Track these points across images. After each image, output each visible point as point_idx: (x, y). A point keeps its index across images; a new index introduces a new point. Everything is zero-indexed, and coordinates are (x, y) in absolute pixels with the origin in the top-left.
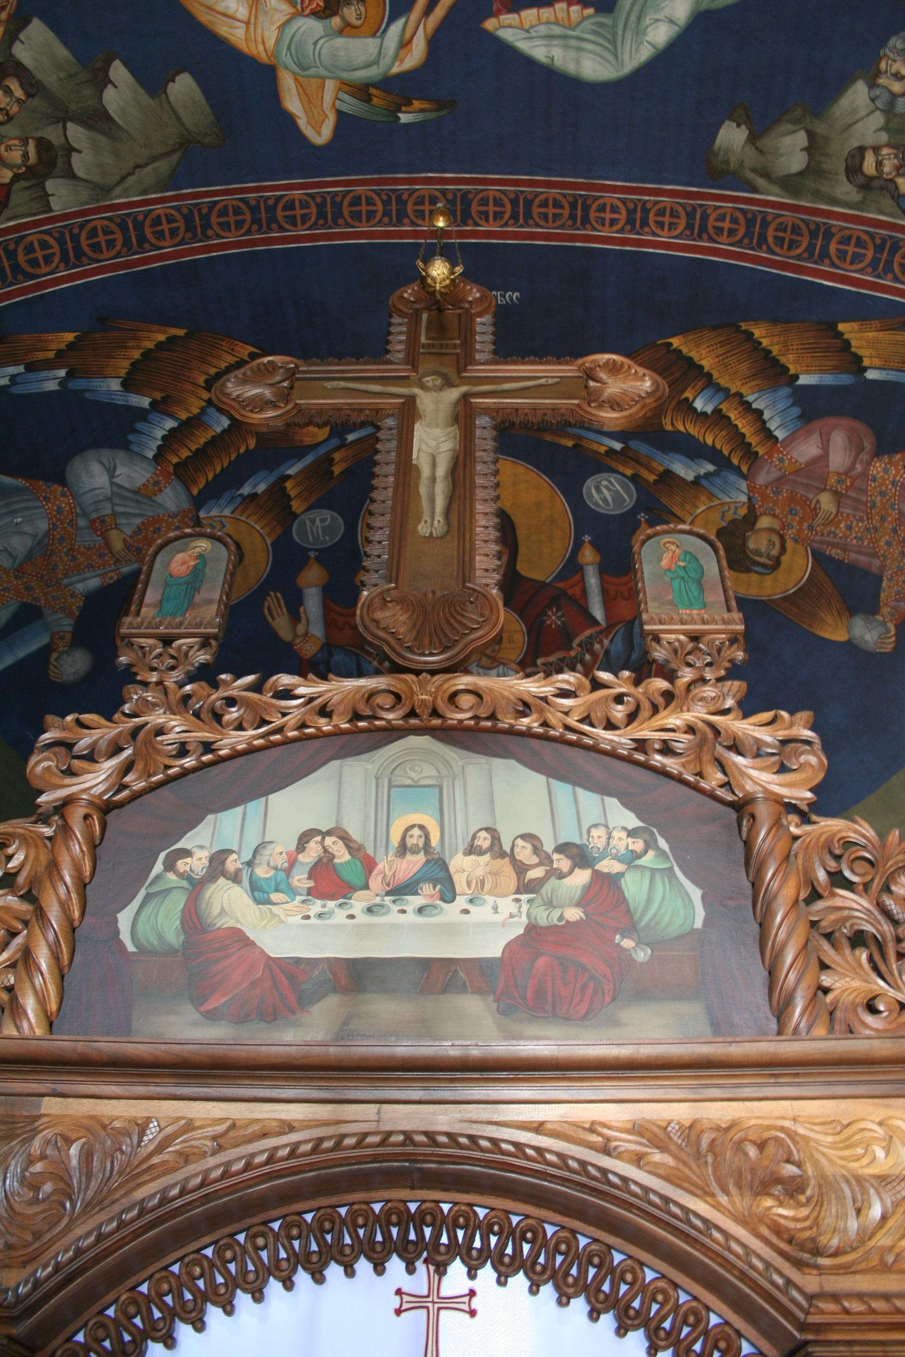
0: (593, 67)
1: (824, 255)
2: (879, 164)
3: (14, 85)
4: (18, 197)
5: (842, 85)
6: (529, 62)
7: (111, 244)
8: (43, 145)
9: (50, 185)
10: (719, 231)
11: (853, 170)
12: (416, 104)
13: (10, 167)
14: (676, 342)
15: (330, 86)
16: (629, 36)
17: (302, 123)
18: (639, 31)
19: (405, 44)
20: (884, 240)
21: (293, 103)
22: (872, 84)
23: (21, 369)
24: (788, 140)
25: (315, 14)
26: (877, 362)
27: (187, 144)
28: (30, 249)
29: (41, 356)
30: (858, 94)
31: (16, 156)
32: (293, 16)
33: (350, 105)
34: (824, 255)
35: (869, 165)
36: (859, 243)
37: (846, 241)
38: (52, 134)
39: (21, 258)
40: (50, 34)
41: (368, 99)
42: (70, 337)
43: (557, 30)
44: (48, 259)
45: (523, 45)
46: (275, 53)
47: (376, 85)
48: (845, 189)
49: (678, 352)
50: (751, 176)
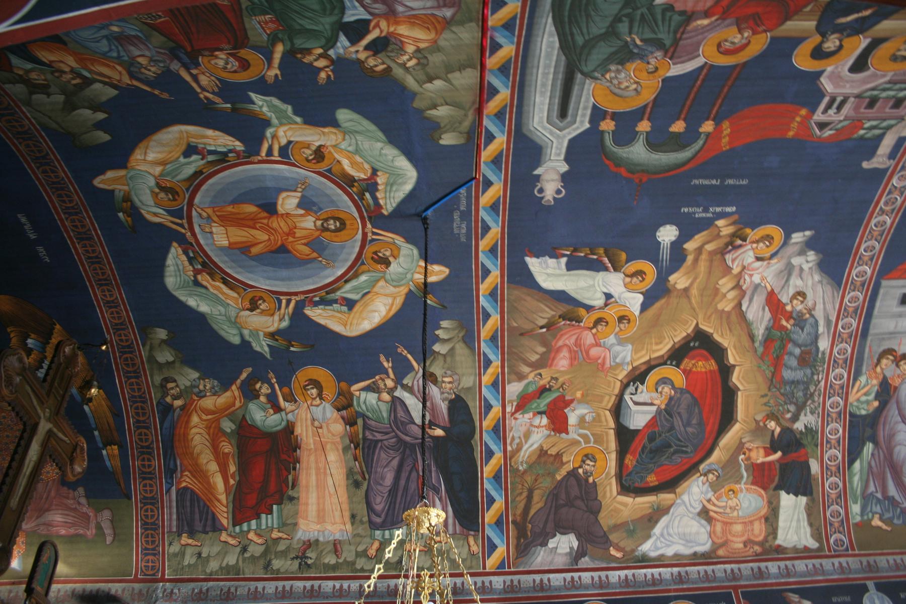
0: (170, 282)
1: (128, 378)
2: (172, 388)
5: (195, 368)
6: (164, 258)
10: (120, 335)
11: (167, 380)
14: (58, 327)
15: (126, 188)
17: (102, 177)
18: (190, 295)
20: (145, 397)
21: (110, 174)
22: (199, 378)
24: (168, 354)
26: (93, 408)
30: (195, 375)
32: (154, 176)
34: (128, 378)
35: (170, 385)
36: (139, 389)
37: (138, 384)
45: (170, 256)
46: (133, 168)
48: (158, 379)
49: (54, 329)
50: (148, 343)
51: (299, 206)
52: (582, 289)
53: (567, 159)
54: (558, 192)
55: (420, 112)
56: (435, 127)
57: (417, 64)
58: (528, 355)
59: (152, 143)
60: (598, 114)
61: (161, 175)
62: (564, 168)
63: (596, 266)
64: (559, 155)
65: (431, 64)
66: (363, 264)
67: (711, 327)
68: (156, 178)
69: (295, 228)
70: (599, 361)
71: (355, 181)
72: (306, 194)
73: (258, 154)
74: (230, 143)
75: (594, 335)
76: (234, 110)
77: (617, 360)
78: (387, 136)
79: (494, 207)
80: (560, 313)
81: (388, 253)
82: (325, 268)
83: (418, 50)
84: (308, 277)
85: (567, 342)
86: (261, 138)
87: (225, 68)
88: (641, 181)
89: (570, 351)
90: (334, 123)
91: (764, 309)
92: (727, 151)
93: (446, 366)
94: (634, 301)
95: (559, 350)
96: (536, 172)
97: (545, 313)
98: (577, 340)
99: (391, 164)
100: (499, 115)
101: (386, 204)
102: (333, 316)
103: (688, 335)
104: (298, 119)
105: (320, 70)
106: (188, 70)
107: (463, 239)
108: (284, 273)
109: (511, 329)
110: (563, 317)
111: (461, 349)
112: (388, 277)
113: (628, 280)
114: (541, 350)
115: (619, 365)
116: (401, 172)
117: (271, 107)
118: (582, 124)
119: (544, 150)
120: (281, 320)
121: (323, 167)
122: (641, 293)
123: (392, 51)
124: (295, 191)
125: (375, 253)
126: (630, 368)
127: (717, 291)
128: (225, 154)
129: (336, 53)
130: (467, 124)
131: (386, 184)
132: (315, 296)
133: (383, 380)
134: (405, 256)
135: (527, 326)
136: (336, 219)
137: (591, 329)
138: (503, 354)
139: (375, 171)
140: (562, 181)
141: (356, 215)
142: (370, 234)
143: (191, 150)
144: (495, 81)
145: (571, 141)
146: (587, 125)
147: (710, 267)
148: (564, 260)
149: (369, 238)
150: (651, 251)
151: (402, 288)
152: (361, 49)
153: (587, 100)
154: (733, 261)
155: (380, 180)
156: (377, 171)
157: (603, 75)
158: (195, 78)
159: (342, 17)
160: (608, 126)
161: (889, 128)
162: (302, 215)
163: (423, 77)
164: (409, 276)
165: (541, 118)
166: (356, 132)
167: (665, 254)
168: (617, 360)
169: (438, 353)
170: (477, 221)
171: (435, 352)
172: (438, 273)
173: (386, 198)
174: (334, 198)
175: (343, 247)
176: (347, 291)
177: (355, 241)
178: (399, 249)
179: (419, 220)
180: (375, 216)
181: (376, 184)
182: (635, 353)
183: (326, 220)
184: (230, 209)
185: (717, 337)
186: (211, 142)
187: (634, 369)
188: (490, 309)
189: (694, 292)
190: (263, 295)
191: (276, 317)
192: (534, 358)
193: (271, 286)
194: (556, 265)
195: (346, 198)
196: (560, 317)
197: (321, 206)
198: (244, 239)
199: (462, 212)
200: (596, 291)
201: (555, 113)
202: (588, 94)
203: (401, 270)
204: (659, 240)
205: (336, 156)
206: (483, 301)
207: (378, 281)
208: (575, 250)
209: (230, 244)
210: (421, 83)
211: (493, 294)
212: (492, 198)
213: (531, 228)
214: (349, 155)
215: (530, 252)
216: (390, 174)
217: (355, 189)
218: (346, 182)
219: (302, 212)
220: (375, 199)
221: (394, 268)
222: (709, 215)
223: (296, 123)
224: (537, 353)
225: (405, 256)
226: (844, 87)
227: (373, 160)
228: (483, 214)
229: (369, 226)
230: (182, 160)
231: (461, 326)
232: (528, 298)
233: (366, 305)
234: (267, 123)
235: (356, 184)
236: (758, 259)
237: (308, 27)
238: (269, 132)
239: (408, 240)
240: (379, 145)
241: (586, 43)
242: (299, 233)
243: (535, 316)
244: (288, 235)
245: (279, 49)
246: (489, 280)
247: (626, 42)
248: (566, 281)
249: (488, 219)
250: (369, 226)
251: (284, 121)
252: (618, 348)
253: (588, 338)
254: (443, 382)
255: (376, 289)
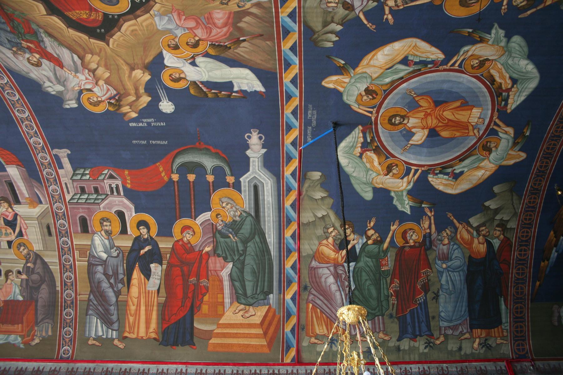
3: (482, 229)
4: (508, 235)
6: (524, 101)
7: (531, 215)
8: (498, 226)
9: (508, 227)
12: (525, 131)
13: (500, 235)
15: (511, 152)
16: (528, 75)
17: (518, 160)
19: (506, 133)
21: (512, 162)
23: (555, 249)
25: (490, 154)
27: (511, 191)
28: (523, 236)
29: (554, 242)
31: (498, 233)
33: (518, 148)
38: (496, 223)
39: (524, 239)
40: (473, 217)
41: (518, 143)
42: (552, 232)
43: (518, 94)
44: (527, 232)
45: (518, 103)
46: (496, 165)
47: (515, 140)
51: (413, 134)
52: (217, 69)
53: (248, 158)
54: (249, 137)
55: (330, 196)
56: (324, 185)
57: (328, 229)
58: (253, 21)
59: (474, 182)
60: (237, 186)
61: (484, 160)
62: (248, 153)
63: (210, 85)
64: (253, 161)
65: (322, 228)
66: (385, 91)
67: (94, 43)
68: (488, 158)
69: (422, 118)
70: (184, 17)
71: (374, 150)
72: (406, 143)
73: (423, 171)
74: (434, 180)
75: (196, 35)
76: (422, 203)
77: (167, 18)
78: (349, 180)
79: (289, 128)
80: (231, 51)
81: (365, 98)
82: (413, 89)
83: (327, 238)
84: (429, 82)
85: (219, 30)
86: (416, 183)
87: (414, 232)
88: (200, 144)
89: (215, 24)
90: (376, 190)
91: (58, 55)
92: (157, 162)
93: (331, 15)
94: (170, 60)
95: (225, 25)
96: (265, 150)
97: (243, 50)
98: (211, 32)
99: (351, 161)
100: (289, 190)
101: (359, 133)
102: (423, 53)
103: (111, 36)
104: (393, 194)
105: (372, 228)
106: (430, 233)
107: (310, 106)
108: (445, 86)
109: (271, 38)
110: (227, 48)
111: (317, 24)
112: (369, 80)
113: (182, 76)
114: (241, 25)
115: (164, 14)
116: (345, 155)
117: (402, 204)
118: (244, 180)
119: (262, 164)
120: (468, 51)
121: (391, 160)
122: (168, 67)
123: (339, 239)
124: (412, 145)
125: (374, 98)
126: (152, 12)
127: (107, 67)
128: (441, 173)
129: (362, 239)
130: (306, 185)
131: (356, 147)
132: (431, 68)
133: (397, 6)
134: (352, 95)
135: (257, 41)
136: (394, 124)
137: (200, 40)
138: (278, 22)
139: (361, 156)
140: (248, 144)
141: (379, 126)
142: (374, 112)
143: (456, 176)
144: (293, 214)
145: (248, 170)
146: (241, 179)
147: (123, 86)
148: (236, 89)
149: (375, 109)
150: (172, 95)
151: (360, 71)
152: (352, 242)
153: (245, 196)
154: (108, 90)
155: (359, 150)
156: (359, 156)
157: (241, 213)
158: (430, 227)
159: (355, 265)
160: (230, 179)
161: (74, 174)
162: (414, 127)
163: (327, 219)
164: (353, 80)
165: (267, 186)
166: (365, 184)
167: (162, 93)
168: (167, 18)
169: (338, 24)
170: (301, 118)
171: (341, 25)
172: (330, 82)
173: (358, 138)
174: (390, 139)
175: (396, 103)
176: (404, 70)
177: (385, 108)
178: (357, 101)
179: (337, 120)
180: (367, 124)
181: (362, 147)
182: (152, 24)
183: (400, 123)
184: (458, 134)
185: (85, 37)
186: (444, 182)
187: (148, 11)
188: (291, 54)
189: (125, 68)
190: (471, 71)
191: (470, 53)
192: (247, 19)
193: (460, 77)
194: (241, 85)
195: (382, 139)
196: (230, 48)
197: (400, 134)
198: (461, 112)
199: (311, 126)
200: (205, 67)
201: (260, 189)
202: (245, 200)
203: (358, 85)
204: (170, 103)
205: (380, 168)
206: (296, 60)
207: (377, 78)
208: (229, 96)
209: (472, 109)
210: (328, 215)
211: (288, 65)
212: (291, 135)
213: (264, 110)
214: (373, 169)
215: (262, 95)
216: (352, 154)
217: (375, 144)
218: (380, 150)
219: (414, 130)
220: (365, 137)
221: (362, 87)
222: (145, 120)
223: (394, 192)
224: (245, 22)
225: (352, 95)
226: (119, 201)
227: (360, 164)
228: (297, 124)
229: (373, 118)
230: (466, 170)
231: (315, 43)
232: (259, 62)
233: (392, 60)
234: (410, 193)
235: (374, 148)
236: (90, 90)
237: (370, 260)
238: (410, 187)
239: (348, 107)
240: (354, 174)
241: (254, 238)
242: (422, 115)
243: (252, 49)
244: (430, 114)
245: (386, 245)
246: (291, 76)
247: (236, 236)
248: (231, 74)
249: (293, 120)
250: (373, 118)
251: (400, 193)
252: (170, 27)
253: (200, 33)
254: (337, 3)
255: (382, 71)
